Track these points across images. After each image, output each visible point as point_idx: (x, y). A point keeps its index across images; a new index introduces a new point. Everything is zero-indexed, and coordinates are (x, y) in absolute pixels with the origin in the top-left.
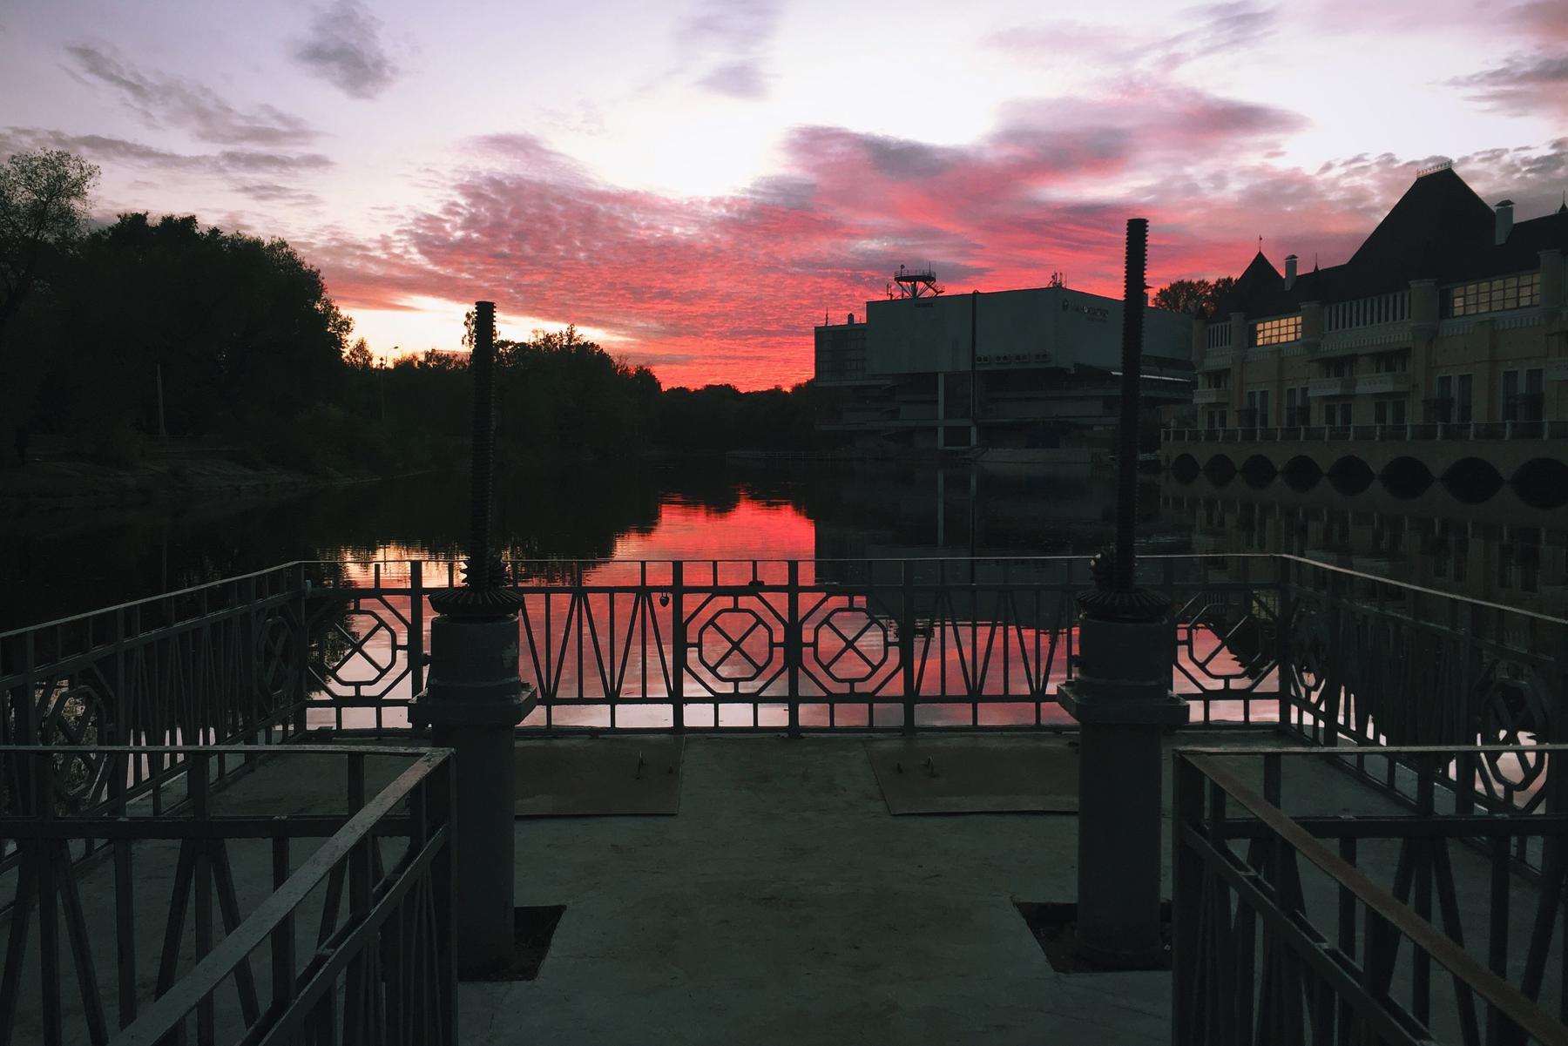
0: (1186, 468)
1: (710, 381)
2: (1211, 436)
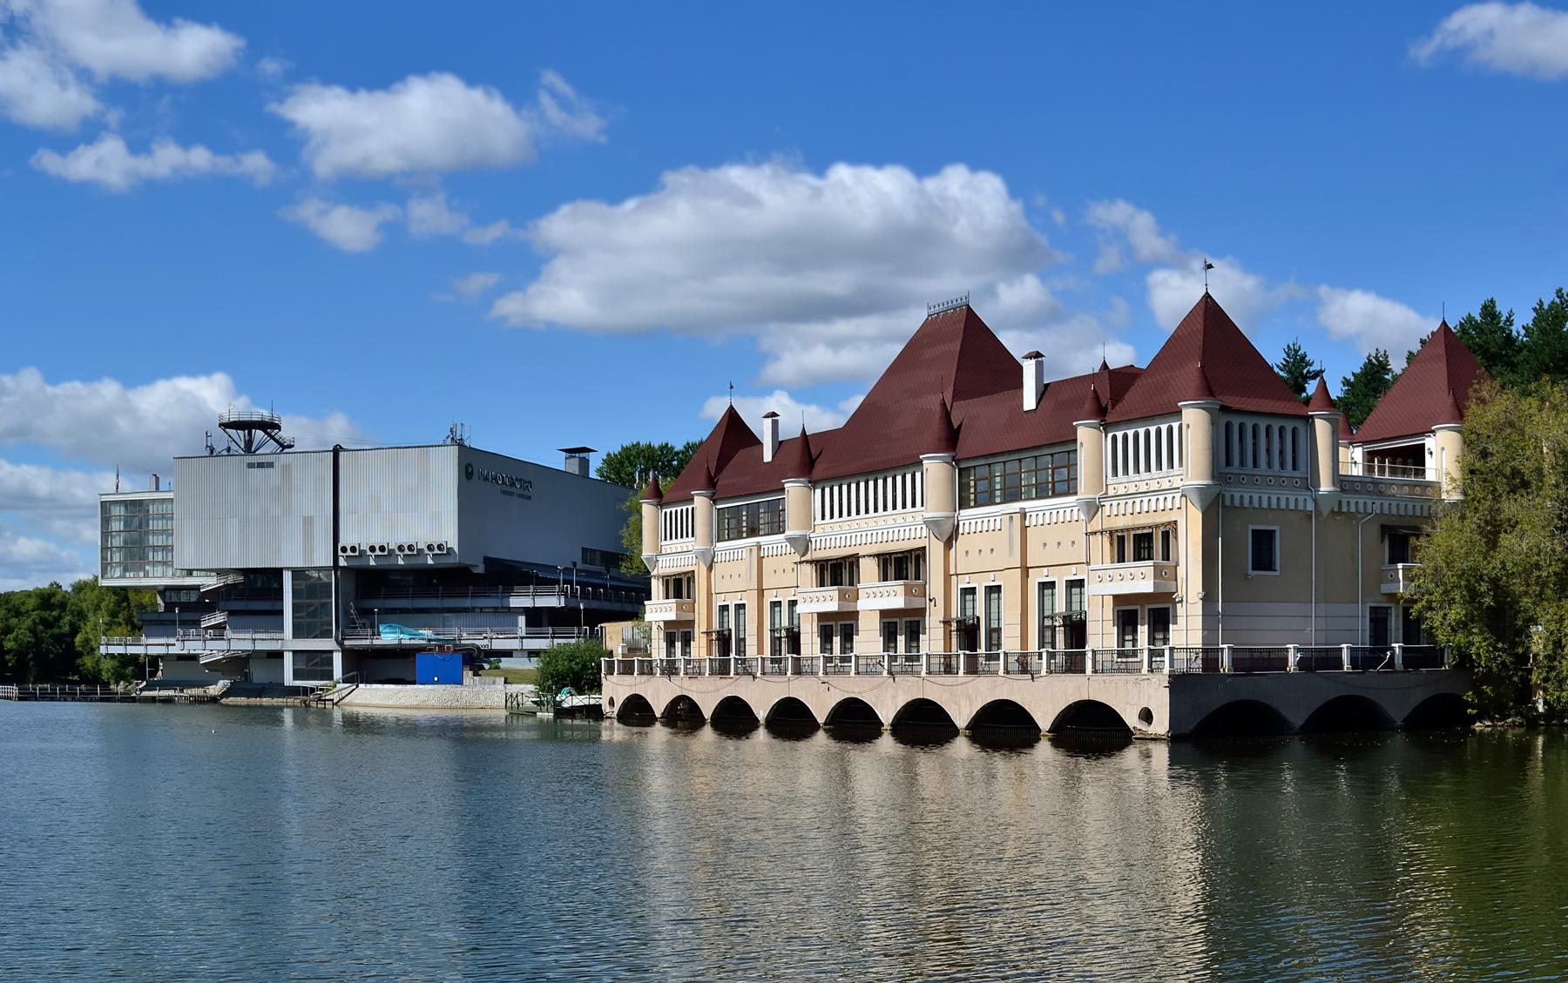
0: (636, 711)
1: (1445, 389)
2: (670, 669)
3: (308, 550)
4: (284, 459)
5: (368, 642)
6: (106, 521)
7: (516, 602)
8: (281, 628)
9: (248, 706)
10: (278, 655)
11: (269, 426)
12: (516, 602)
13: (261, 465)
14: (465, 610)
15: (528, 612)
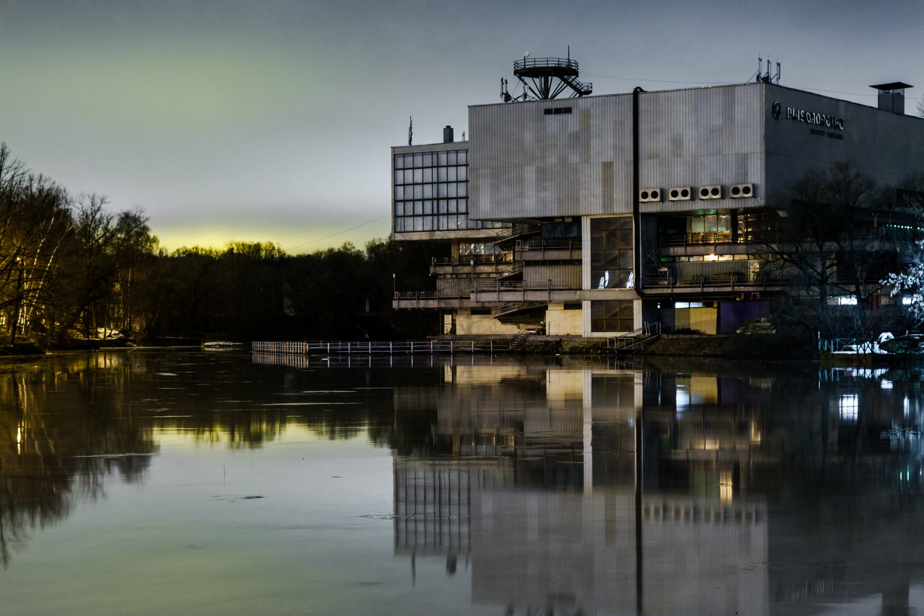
3: (608, 200)
4: (583, 102)
11: (567, 72)
13: (558, 111)
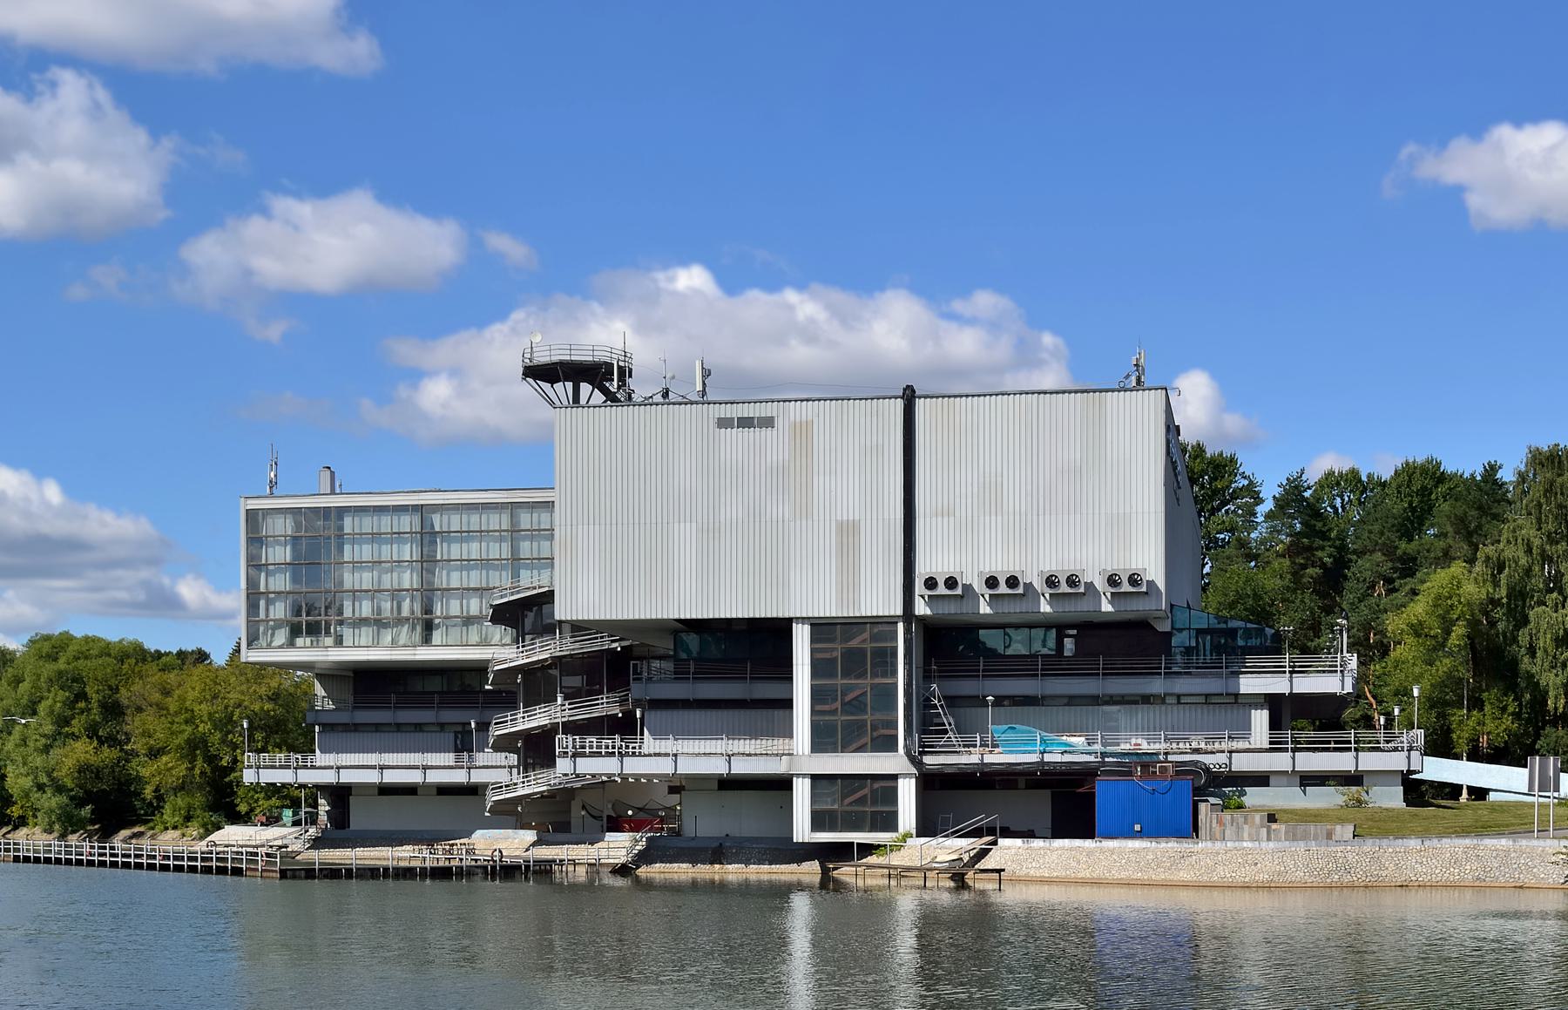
5: (974, 759)
6: (255, 540)
7: (1249, 684)
8: (788, 732)
9: (694, 885)
10: (783, 784)
12: (1249, 684)
13: (745, 423)
14: (1146, 699)
15: (1273, 702)
